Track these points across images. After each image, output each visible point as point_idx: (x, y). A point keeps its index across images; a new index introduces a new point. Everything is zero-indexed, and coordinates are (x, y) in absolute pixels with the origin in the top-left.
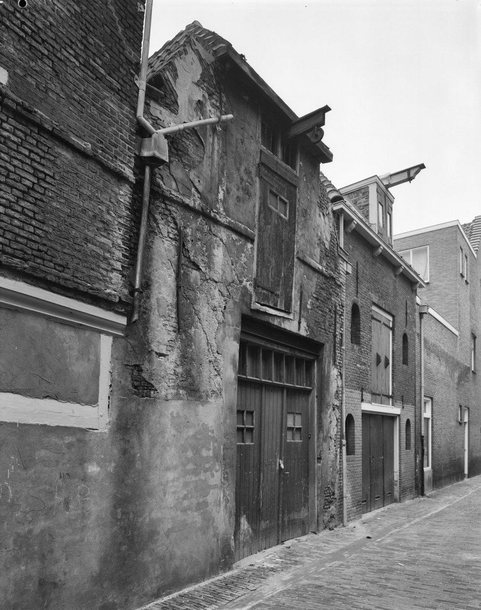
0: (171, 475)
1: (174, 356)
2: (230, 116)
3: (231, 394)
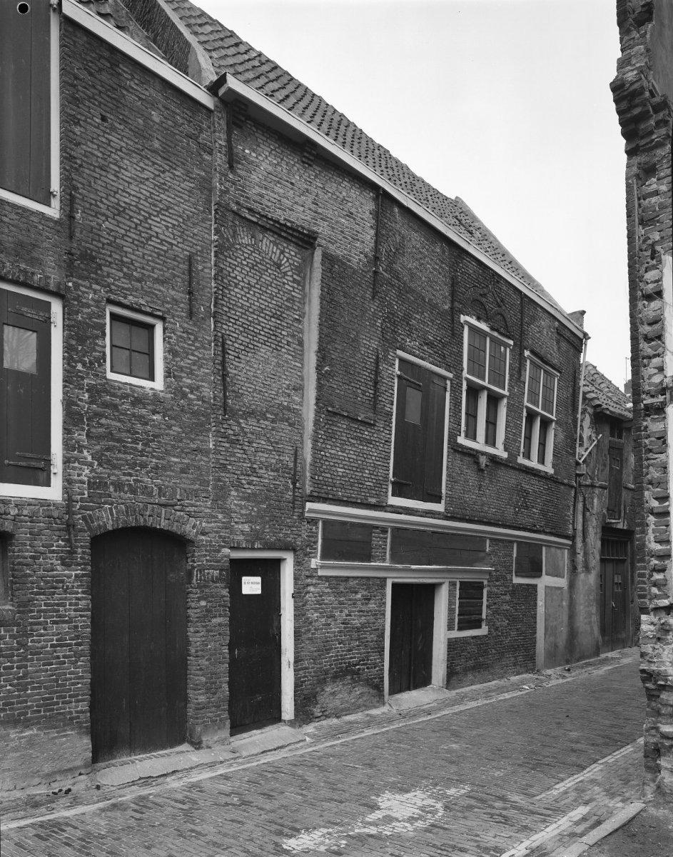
0: (582, 607)
1: (582, 554)
2: (601, 435)
3: (598, 568)
